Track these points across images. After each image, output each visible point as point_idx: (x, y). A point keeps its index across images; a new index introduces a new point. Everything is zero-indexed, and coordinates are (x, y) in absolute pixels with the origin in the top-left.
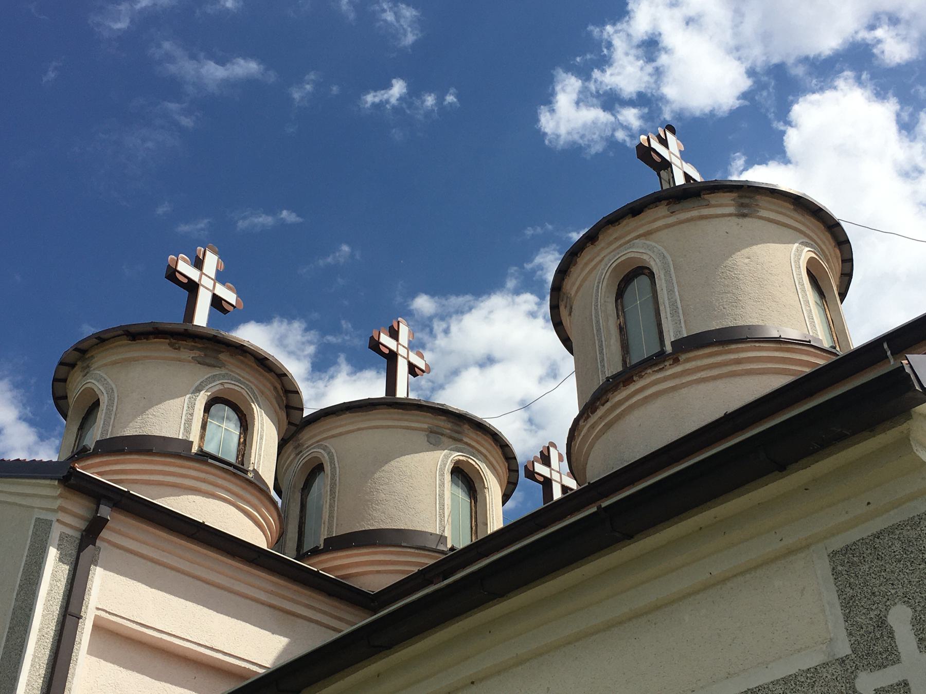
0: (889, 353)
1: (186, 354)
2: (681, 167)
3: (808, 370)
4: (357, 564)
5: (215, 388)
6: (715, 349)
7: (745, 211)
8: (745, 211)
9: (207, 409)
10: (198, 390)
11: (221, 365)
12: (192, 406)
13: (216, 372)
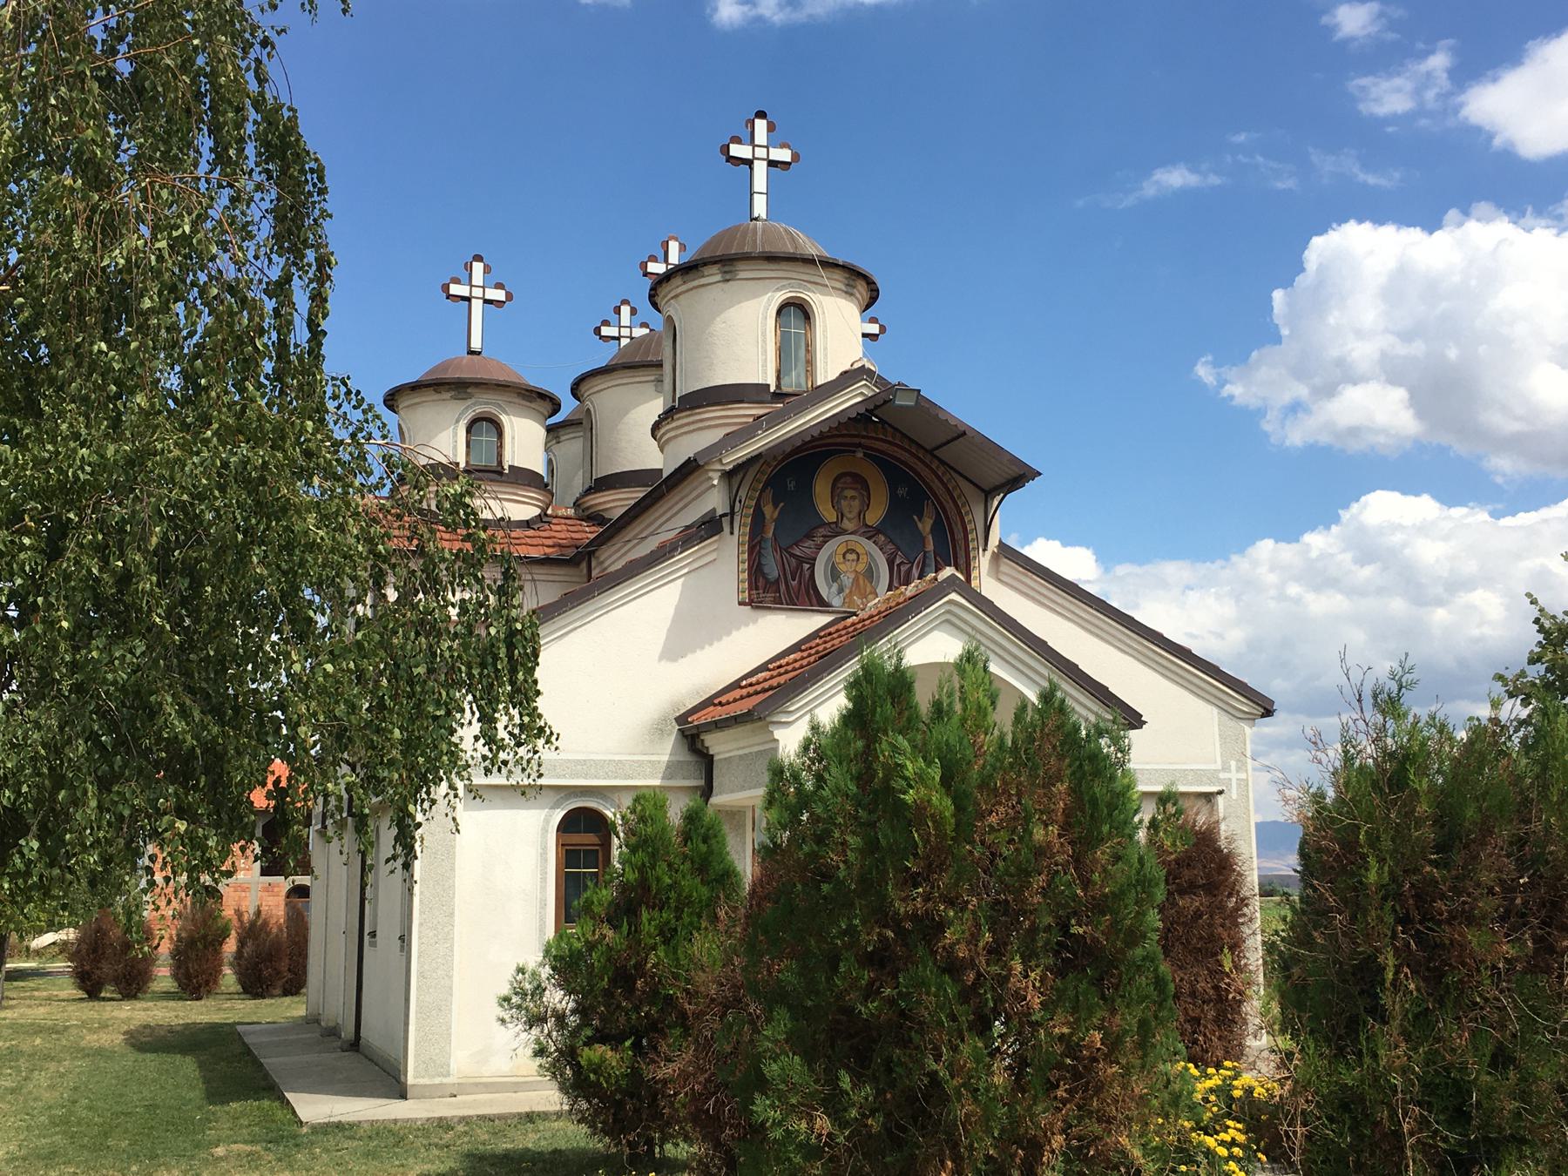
0: (230, 946)
1: (447, 395)
2: (639, 493)
3: (633, 502)
4: (609, 502)
5: (470, 415)
6: (688, 413)
7: (728, 277)
8: (728, 277)
9: (468, 431)
10: (457, 421)
11: (470, 396)
12: (455, 435)
13: (469, 402)
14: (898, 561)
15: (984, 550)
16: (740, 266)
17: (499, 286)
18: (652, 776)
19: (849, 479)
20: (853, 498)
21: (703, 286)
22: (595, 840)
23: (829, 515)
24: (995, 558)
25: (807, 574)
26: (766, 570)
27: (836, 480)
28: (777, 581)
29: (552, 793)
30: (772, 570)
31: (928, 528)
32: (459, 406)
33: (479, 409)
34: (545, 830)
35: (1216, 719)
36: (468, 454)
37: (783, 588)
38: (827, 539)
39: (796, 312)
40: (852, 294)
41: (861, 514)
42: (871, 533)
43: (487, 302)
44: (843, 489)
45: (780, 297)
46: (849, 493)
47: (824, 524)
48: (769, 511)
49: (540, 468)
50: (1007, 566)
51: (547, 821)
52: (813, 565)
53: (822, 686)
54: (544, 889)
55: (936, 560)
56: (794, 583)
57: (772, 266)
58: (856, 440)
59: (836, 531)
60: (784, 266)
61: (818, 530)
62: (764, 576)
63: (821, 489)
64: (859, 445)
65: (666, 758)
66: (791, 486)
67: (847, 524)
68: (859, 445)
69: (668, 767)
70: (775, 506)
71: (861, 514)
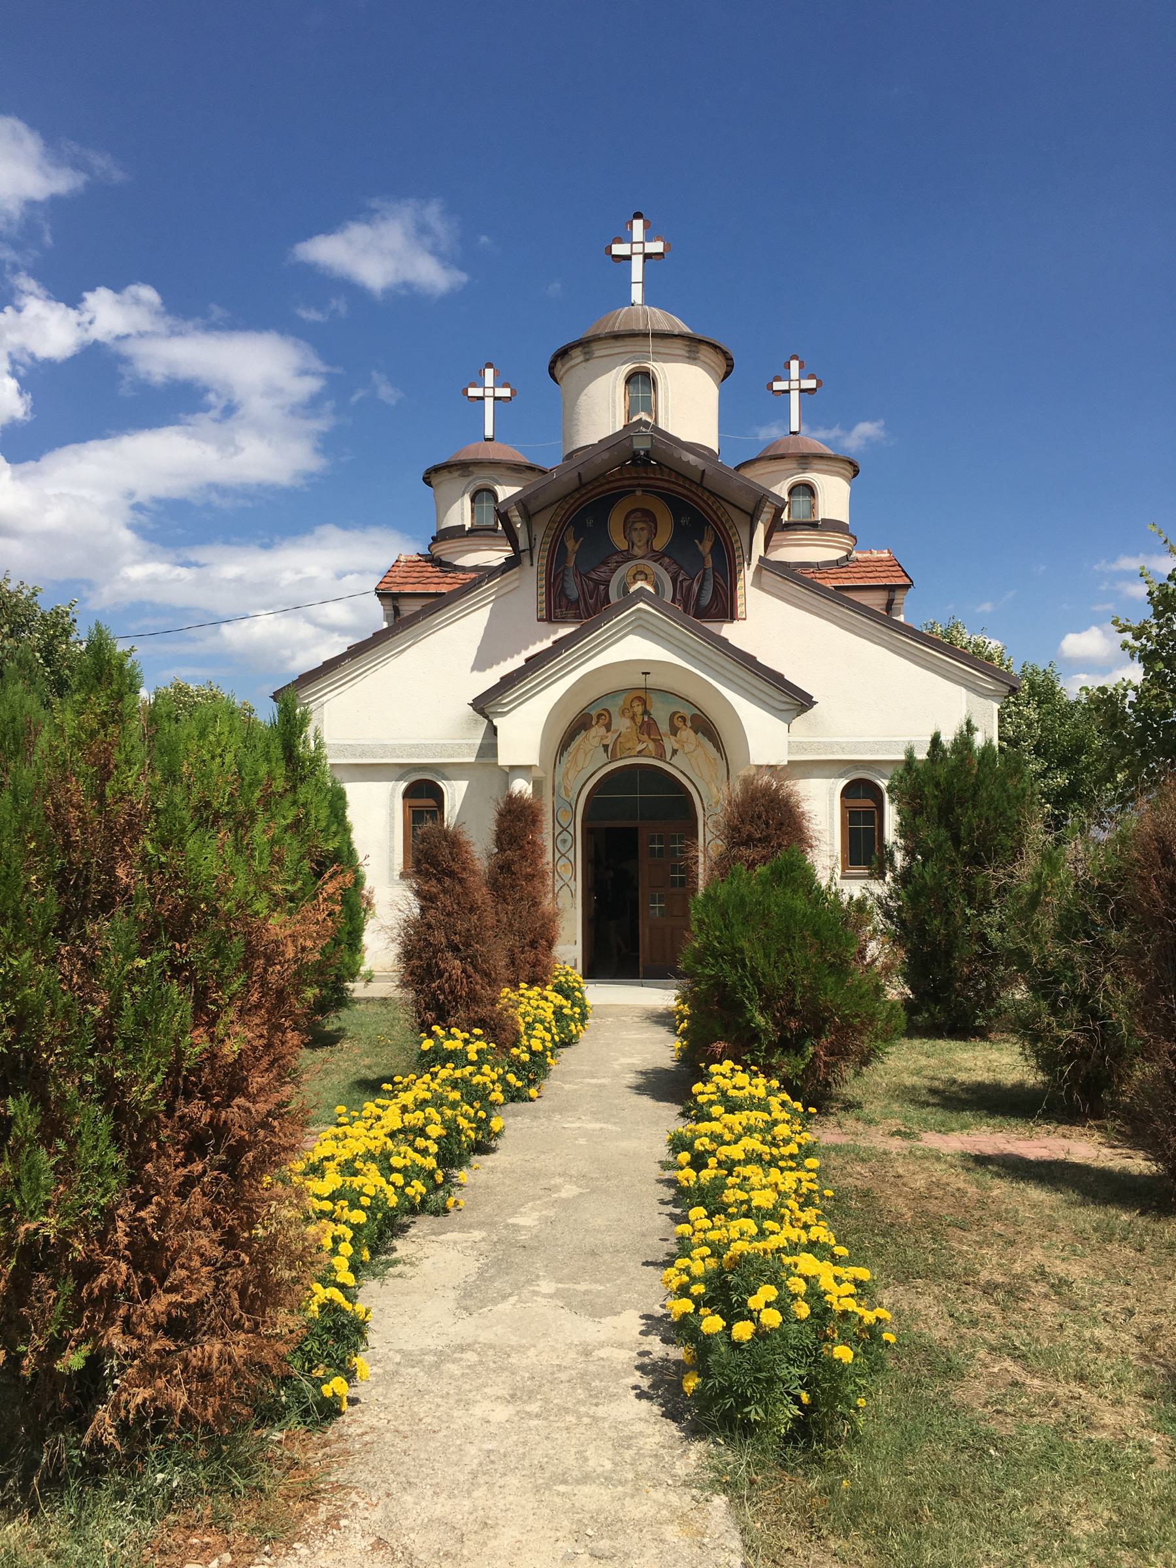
1: (456, 474)
5: (472, 488)
9: (473, 501)
11: (473, 473)
12: (462, 504)
13: (471, 478)
14: (680, 578)
15: (749, 564)
16: (595, 346)
17: (811, 377)
18: (469, 755)
19: (639, 514)
20: (642, 529)
21: (572, 367)
22: (872, 804)
23: (621, 543)
24: (759, 569)
25: (603, 593)
26: (568, 592)
27: (627, 517)
28: (577, 601)
29: (397, 769)
30: (573, 592)
31: (708, 550)
32: (464, 481)
33: (479, 483)
34: (392, 796)
35: (964, 698)
36: (472, 517)
37: (582, 605)
38: (619, 564)
39: (641, 380)
40: (695, 359)
41: (649, 542)
42: (657, 557)
43: (496, 399)
44: (634, 522)
45: (627, 368)
46: (639, 525)
47: (617, 552)
48: (571, 545)
49: (845, 519)
50: (767, 576)
51: (394, 790)
52: (608, 586)
53: (529, 682)
54: (392, 838)
55: (714, 576)
56: (591, 601)
57: (619, 343)
58: (636, 482)
59: (628, 557)
60: (628, 341)
61: (611, 557)
62: (566, 596)
63: (615, 524)
64: (639, 485)
65: (479, 741)
66: (590, 523)
67: (637, 551)
68: (639, 485)
69: (481, 748)
70: (576, 541)
71: (649, 542)
